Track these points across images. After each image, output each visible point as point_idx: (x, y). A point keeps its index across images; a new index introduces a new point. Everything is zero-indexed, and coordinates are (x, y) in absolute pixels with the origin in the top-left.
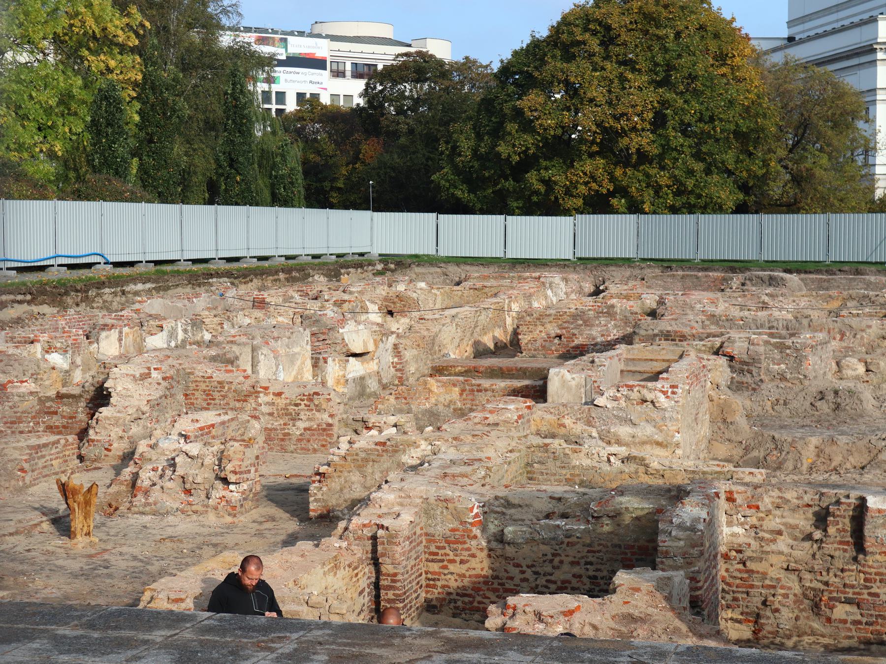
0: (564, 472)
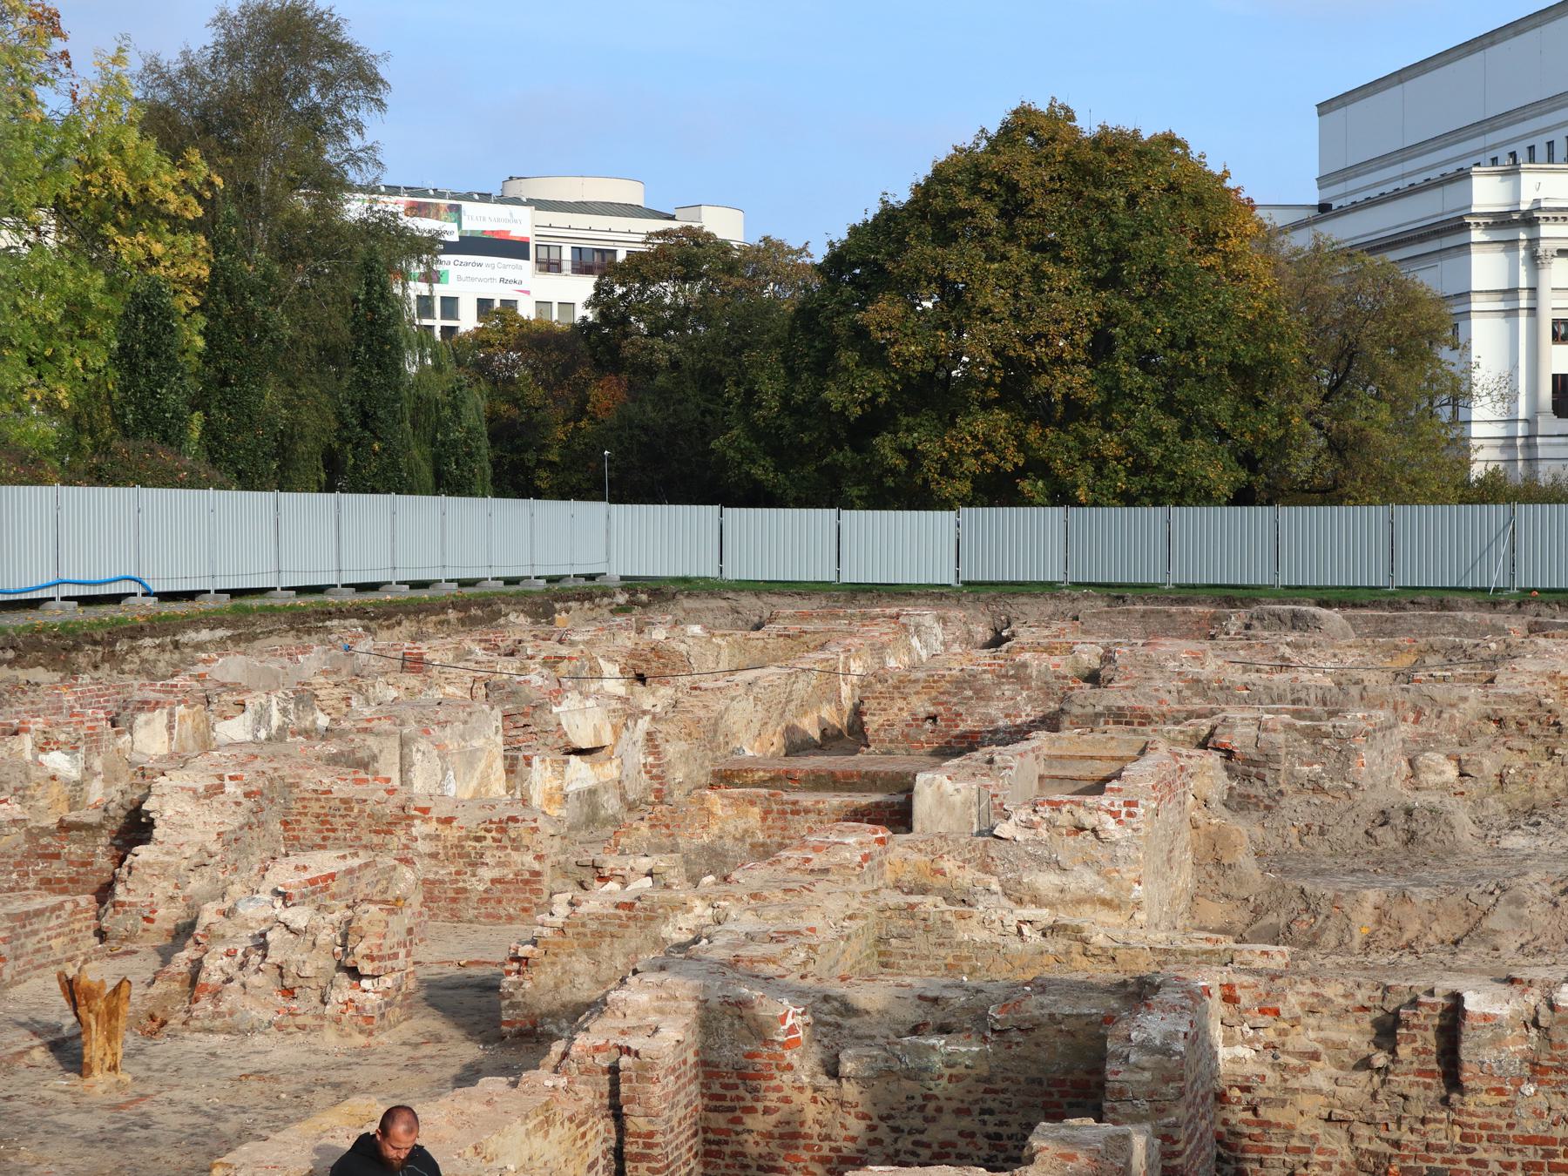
0: (943, 952)
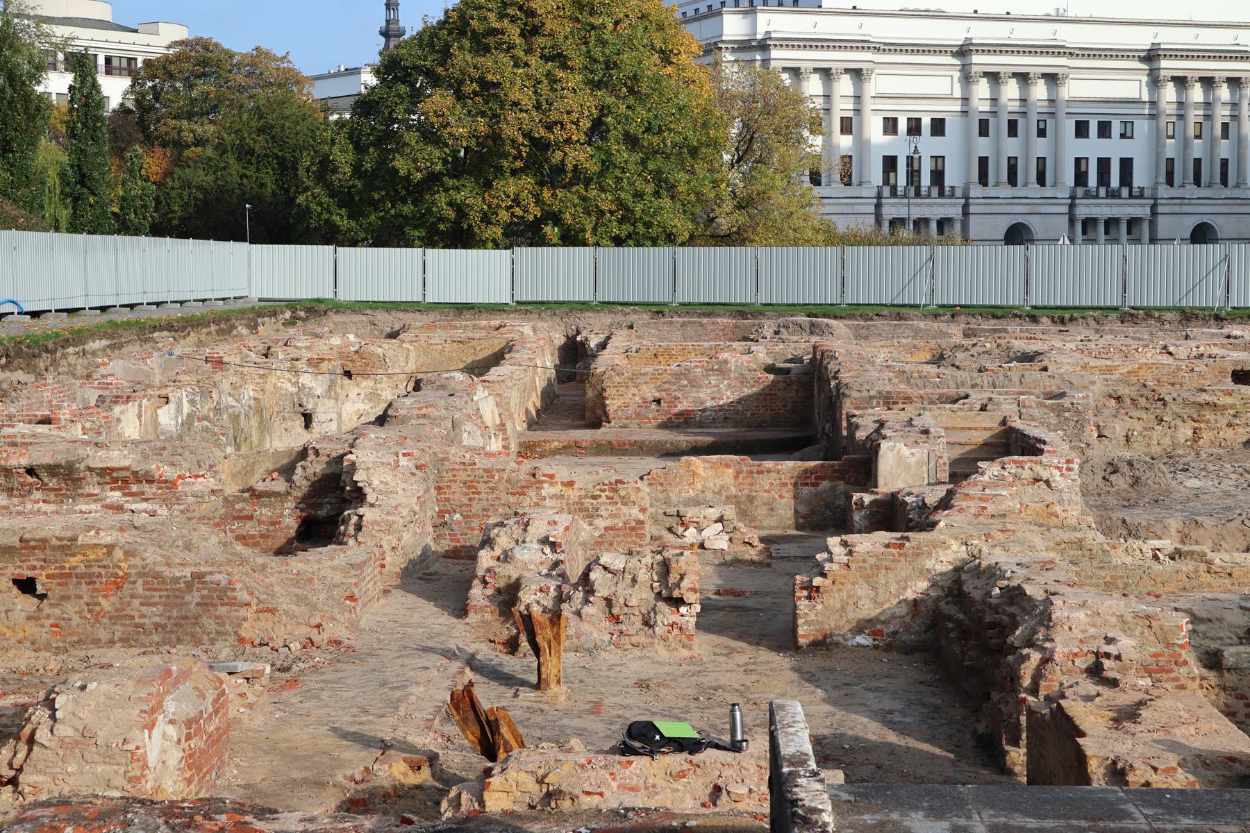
0: (1103, 573)
